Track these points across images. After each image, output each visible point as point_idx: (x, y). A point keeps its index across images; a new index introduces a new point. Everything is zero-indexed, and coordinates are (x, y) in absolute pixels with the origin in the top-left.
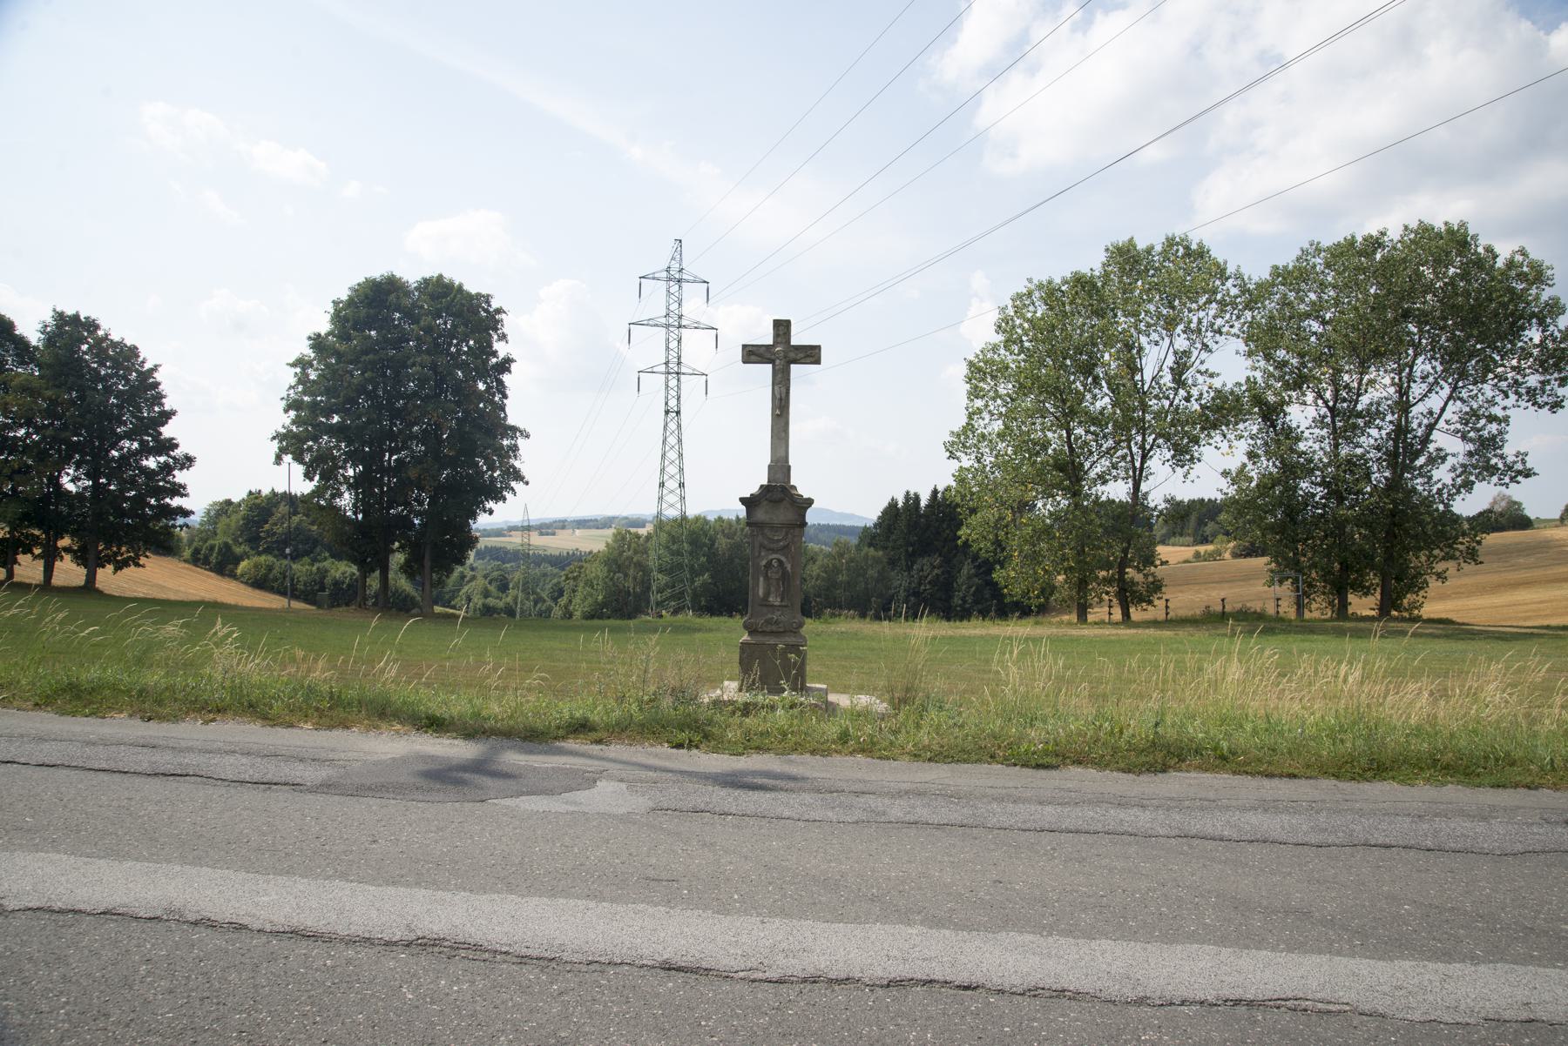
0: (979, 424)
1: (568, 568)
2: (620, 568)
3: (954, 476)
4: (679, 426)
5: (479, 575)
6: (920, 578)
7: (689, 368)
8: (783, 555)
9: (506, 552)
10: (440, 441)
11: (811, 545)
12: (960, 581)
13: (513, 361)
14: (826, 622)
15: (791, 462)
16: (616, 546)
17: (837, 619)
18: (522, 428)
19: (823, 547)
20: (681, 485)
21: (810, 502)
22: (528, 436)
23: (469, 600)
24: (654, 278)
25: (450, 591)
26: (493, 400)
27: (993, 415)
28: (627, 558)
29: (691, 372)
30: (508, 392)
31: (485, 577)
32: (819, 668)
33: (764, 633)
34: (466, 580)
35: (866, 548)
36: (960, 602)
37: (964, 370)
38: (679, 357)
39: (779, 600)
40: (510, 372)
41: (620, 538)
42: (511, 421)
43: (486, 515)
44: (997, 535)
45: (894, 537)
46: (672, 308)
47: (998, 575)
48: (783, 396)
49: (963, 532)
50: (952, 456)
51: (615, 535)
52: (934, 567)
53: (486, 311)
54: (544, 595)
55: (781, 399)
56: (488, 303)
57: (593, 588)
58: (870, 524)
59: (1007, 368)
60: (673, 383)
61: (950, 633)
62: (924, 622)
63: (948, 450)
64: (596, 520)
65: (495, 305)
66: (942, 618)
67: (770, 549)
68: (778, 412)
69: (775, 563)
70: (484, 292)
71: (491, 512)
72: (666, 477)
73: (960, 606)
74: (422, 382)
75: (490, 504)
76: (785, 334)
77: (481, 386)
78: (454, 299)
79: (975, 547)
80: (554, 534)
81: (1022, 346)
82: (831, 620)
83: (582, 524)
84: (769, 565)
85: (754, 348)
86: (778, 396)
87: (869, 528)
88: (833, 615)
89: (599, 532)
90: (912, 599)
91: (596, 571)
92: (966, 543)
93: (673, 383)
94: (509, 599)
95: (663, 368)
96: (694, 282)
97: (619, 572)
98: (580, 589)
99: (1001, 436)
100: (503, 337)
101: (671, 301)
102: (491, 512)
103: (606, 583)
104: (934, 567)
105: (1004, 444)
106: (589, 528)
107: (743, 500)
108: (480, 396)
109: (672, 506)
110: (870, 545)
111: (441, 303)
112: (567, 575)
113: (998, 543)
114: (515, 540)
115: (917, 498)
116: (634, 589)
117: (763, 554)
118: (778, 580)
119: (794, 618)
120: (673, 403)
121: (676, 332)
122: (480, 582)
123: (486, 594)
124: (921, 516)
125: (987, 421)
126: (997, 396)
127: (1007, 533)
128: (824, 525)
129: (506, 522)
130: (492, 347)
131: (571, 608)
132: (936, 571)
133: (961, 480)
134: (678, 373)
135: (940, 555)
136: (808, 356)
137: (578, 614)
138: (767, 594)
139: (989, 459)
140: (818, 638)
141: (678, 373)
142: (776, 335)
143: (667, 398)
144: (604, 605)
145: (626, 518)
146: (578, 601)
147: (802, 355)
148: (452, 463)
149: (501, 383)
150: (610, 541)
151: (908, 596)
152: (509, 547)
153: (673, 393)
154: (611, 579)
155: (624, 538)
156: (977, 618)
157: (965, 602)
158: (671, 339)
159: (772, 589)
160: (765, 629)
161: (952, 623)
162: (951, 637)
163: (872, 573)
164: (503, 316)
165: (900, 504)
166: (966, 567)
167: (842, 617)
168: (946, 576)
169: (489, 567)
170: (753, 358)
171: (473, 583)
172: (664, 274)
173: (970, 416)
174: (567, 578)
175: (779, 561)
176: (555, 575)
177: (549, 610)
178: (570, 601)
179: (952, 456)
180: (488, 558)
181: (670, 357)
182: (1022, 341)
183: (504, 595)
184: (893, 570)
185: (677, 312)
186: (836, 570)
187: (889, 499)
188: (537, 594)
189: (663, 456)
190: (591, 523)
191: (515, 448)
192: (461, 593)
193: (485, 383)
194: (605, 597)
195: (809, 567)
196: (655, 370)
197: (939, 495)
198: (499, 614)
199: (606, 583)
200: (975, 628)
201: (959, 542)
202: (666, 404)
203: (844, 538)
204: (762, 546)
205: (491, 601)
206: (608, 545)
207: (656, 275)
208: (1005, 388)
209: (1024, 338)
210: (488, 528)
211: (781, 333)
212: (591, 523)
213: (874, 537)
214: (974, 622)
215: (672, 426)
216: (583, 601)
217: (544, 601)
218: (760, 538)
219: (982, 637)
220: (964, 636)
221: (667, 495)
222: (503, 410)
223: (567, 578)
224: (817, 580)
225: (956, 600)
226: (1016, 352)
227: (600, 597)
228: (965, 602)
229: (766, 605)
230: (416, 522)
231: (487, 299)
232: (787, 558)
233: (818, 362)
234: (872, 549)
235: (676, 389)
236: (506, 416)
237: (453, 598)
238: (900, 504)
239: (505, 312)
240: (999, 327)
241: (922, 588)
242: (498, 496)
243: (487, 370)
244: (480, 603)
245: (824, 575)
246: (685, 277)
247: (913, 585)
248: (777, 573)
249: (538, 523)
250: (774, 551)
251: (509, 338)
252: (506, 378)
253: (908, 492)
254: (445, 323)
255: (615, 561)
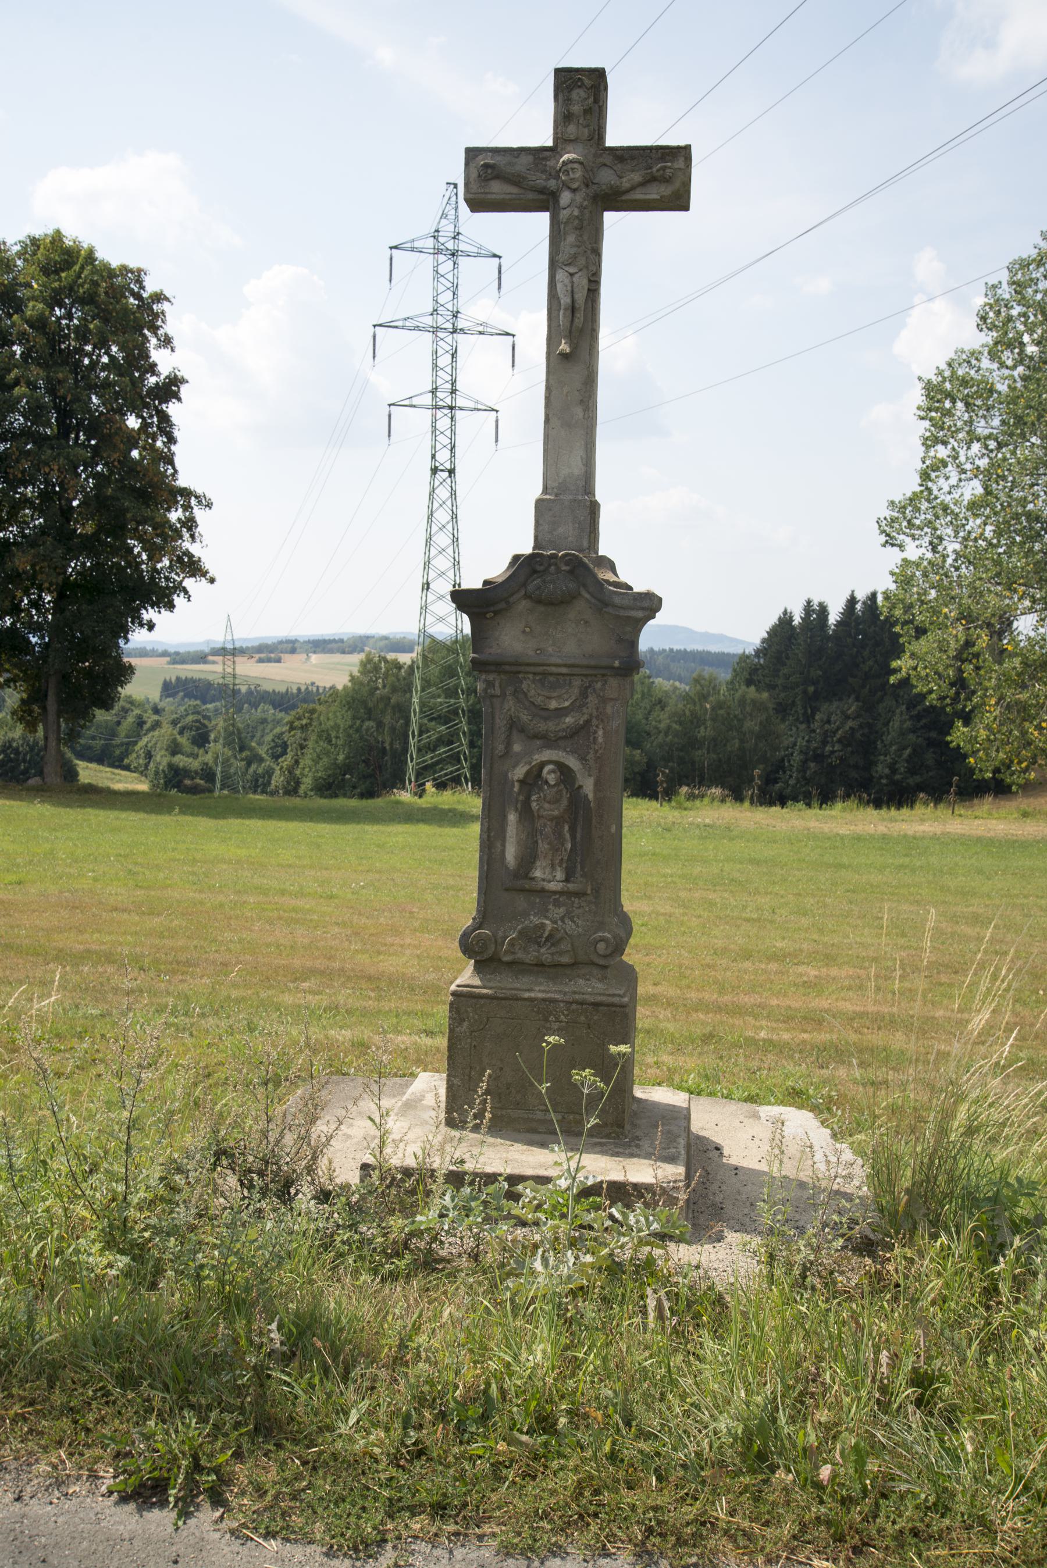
0: (941, 486)
1: (293, 713)
2: (370, 714)
3: (892, 574)
4: (453, 494)
5: (165, 720)
6: (825, 734)
7: (468, 398)
8: (573, 752)
9: (209, 685)
10: (67, 512)
11: (658, 681)
12: (887, 739)
13: (183, 381)
14: (680, 807)
15: (601, 494)
16: (365, 680)
17: (698, 802)
18: (199, 491)
19: (677, 684)
20: (427, 586)
21: (650, 604)
22: (209, 505)
23: (149, 756)
24: (413, 249)
25: (122, 744)
26: (153, 446)
27: (964, 471)
28: (382, 698)
29: (472, 405)
30: (176, 433)
31: (174, 723)
32: (668, 909)
33: (516, 967)
34: (146, 727)
35: (744, 687)
36: (887, 771)
37: (917, 396)
38: (453, 383)
39: (560, 875)
40: (179, 399)
41: (370, 667)
42: (182, 482)
43: (144, 631)
44: (960, 671)
45: (785, 670)
46: (442, 299)
47: (959, 735)
48: (581, 297)
49: (903, 664)
50: (890, 542)
51: (363, 664)
52: (847, 717)
53: (138, 296)
54: (262, 751)
55: (573, 309)
56: (139, 281)
57: (330, 741)
58: (750, 650)
59: (991, 391)
60: (444, 423)
61: (882, 829)
62: (839, 805)
63: (883, 532)
64: (342, 641)
65: (151, 286)
66: (868, 803)
67: (536, 736)
68: (564, 347)
69: (550, 775)
70: (133, 264)
71: (151, 626)
72: (432, 575)
73: (887, 777)
74: (36, 412)
75: (149, 614)
76: (587, 111)
77: (133, 422)
78: (80, 273)
79: (920, 688)
80: (279, 661)
81: (1022, 352)
82: (689, 804)
83: (320, 646)
84: (533, 780)
85: (498, 160)
86: (565, 300)
87: (748, 657)
88: (691, 797)
89: (338, 658)
90: (812, 765)
91: (336, 718)
92: (906, 682)
93: (444, 423)
94: (209, 758)
95: (427, 399)
96: (478, 255)
97: (369, 719)
98: (310, 744)
99: (974, 506)
100: (167, 342)
101: (441, 288)
102: (151, 626)
103: (349, 736)
104: (847, 717)
105: (978, 521)
106: (331, 651)
107: (462, 599)
108: (132, 439)
109: (441, 619)
110: (749, 683)
111: (60, 280)
112: (291, 723)
113: (960, 683)
114: (213, 671)
115: (823, 610)
116: (391, 744)
117: (517, 748)
118: (558, 821)
119: (601, 926)
120: (443, 456)
121: (449, 339)
122: (166, 731)
123: (175, 749)
124: (829, 638)
125: (953, 481)
126: (973, 437)
127: (978, 668)
128: (679, 652)
129: (208, 642)
130: (148, 357)
131: (298, 772)
132: (850, 723)
133: (904, 579)
134: (451, 408)
135: (857, 699)
136: (652, 180)
137: (307, 782)
138: (528, 859)
139: (952, 547)
140: (668, 835)
141: (451, 408)
142: (563, 118)
143: (434, 447)
144: (347, 768)
145: (386, 638)
146: (309, 762)
147: (637, 177)
148: (89, 545)
149: (164, 418)
150: (356, 673)
151: (805, 762)
152: (210, 678)
153: (443, 440)
154: (358, 730)
155: (376, 668)
156: (926, 804)
157: (894, 771)
158: (440, 352)
159: (543, 846)
160: (520, 955)
161: (883, 812)
162: (884, 837)
163: (751, 725)
164: (165, 306)
165: (797, 620)
166: (897, 718)
167: (706, 800)
168: (866, 731)
169: (182, 708)
170: (498, 189)
171: (156, 733)
172: (430, 243)
173: (925, 476)
174: (292, 728)
175: (562, 768)
176: (279, 722)
177: (269, 773)
178: (297, 762)
179: (890, 542)
180: (181, 694)
181: (440, 382)
182: (1022, 345)
183: (201, 751)
184: (783, 720)
185: (449, 306)
186: (697, 720)
187: (779, 612)
188: (251, 749)
189: (429, 540)
190: (334, 645)
191: (190, 524)
192: (137, 748)
193: (138, 416)
194: (347, 757)
195: (655, 714)
196: (415, 401)
197: (858, 606)
198: (193, 779)
199: (349, 736)
200: (923, 821)
201: (892, 680)
202: (433, 457)
203: (708, 671)
204: (514, 725)
205: (180, 760)
206: (353, 678)
207: (417, 244)
208: (990, 425)
209: (1026, 338)
210: (182, 650)
211: (576, 109)
212: (334, 645)
213: (754, 670)
214: (919, 810)
215: (443, 493)
216: (317, 760)
217: (261, 760)
218: (510, 704)
219: (935, 838)
220: (905, 836)
221: (433, 602)
222: (171, 463)
223: (292, 728)
224: (666, 734)
225: (880, 768)
226: (1010, 363)
227: (341, 757)
228: (894, 771)
229: (522, 890)
230: (34, 640)
231: (138, 276)
232: (583, 759)
233: (679, 201)
234: (753, 688)
235: (448, 433)
236: (176, 471)
237: (126, 754)
238: (797, 620)
239: (167, 299)
240: (984, 319)
241: (828, 748)
242: (164, 599)
243: (142, 398)
244: (165, 762)
245: (677, 727)
246: (462, 247)
247: (814, 745)
248: (557, 801)
249: (256, 644)
250: (549, 741)
251: (176, 342)
252: (172, 409)
253: (809, 602)
254: (69, 316)
255: (364, 703)
